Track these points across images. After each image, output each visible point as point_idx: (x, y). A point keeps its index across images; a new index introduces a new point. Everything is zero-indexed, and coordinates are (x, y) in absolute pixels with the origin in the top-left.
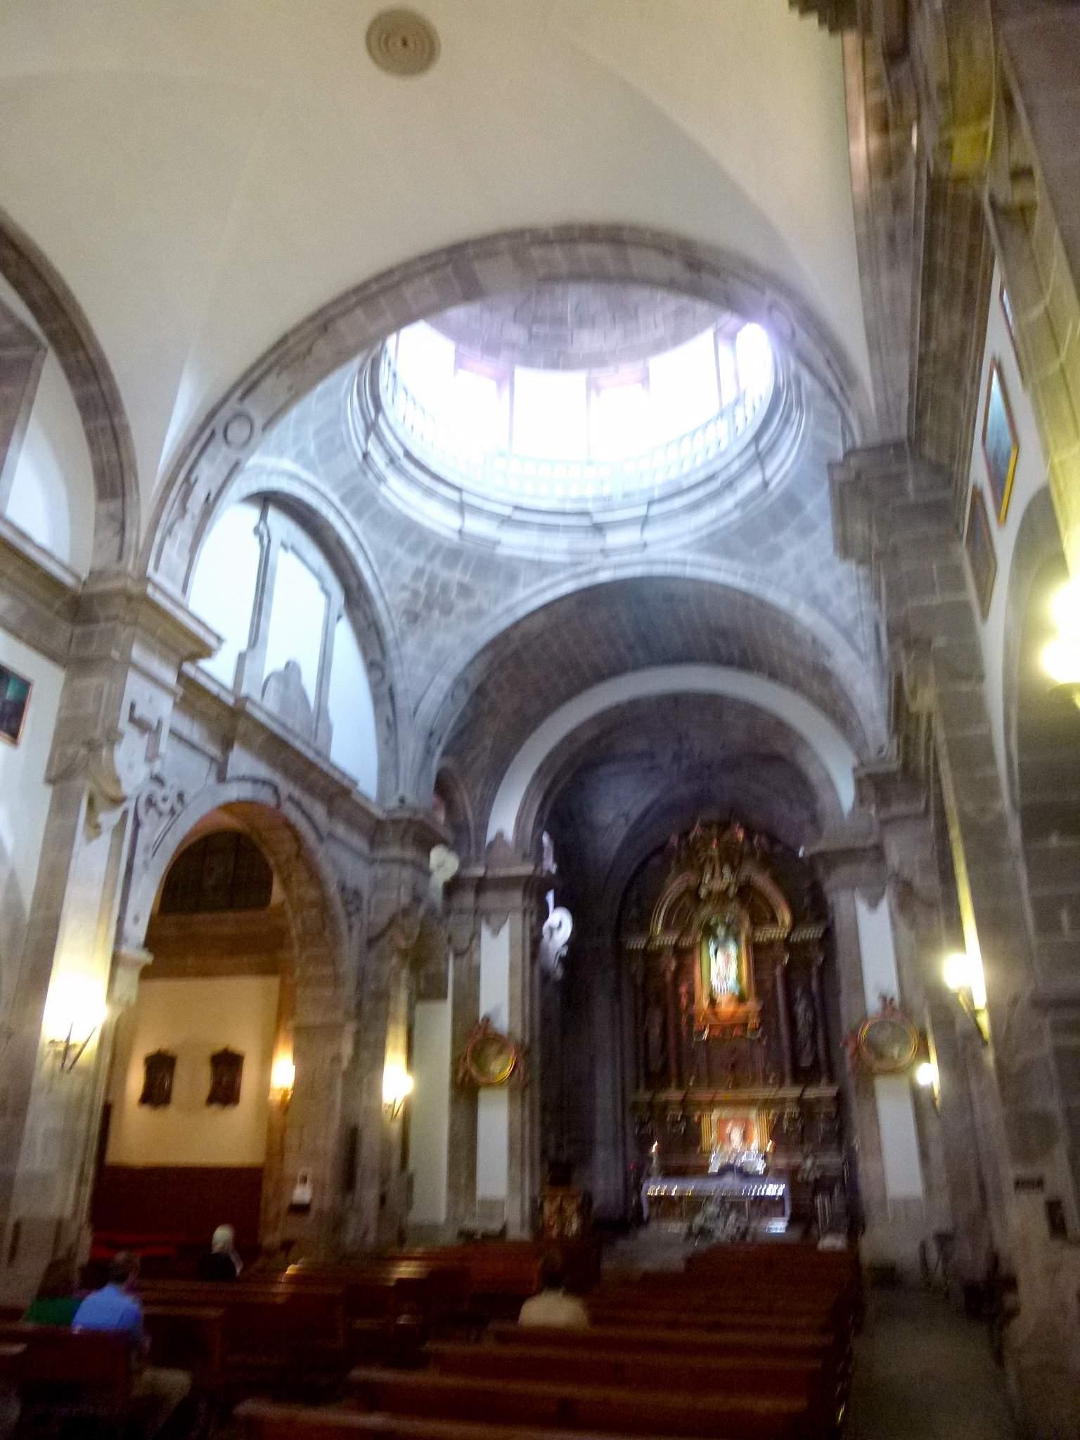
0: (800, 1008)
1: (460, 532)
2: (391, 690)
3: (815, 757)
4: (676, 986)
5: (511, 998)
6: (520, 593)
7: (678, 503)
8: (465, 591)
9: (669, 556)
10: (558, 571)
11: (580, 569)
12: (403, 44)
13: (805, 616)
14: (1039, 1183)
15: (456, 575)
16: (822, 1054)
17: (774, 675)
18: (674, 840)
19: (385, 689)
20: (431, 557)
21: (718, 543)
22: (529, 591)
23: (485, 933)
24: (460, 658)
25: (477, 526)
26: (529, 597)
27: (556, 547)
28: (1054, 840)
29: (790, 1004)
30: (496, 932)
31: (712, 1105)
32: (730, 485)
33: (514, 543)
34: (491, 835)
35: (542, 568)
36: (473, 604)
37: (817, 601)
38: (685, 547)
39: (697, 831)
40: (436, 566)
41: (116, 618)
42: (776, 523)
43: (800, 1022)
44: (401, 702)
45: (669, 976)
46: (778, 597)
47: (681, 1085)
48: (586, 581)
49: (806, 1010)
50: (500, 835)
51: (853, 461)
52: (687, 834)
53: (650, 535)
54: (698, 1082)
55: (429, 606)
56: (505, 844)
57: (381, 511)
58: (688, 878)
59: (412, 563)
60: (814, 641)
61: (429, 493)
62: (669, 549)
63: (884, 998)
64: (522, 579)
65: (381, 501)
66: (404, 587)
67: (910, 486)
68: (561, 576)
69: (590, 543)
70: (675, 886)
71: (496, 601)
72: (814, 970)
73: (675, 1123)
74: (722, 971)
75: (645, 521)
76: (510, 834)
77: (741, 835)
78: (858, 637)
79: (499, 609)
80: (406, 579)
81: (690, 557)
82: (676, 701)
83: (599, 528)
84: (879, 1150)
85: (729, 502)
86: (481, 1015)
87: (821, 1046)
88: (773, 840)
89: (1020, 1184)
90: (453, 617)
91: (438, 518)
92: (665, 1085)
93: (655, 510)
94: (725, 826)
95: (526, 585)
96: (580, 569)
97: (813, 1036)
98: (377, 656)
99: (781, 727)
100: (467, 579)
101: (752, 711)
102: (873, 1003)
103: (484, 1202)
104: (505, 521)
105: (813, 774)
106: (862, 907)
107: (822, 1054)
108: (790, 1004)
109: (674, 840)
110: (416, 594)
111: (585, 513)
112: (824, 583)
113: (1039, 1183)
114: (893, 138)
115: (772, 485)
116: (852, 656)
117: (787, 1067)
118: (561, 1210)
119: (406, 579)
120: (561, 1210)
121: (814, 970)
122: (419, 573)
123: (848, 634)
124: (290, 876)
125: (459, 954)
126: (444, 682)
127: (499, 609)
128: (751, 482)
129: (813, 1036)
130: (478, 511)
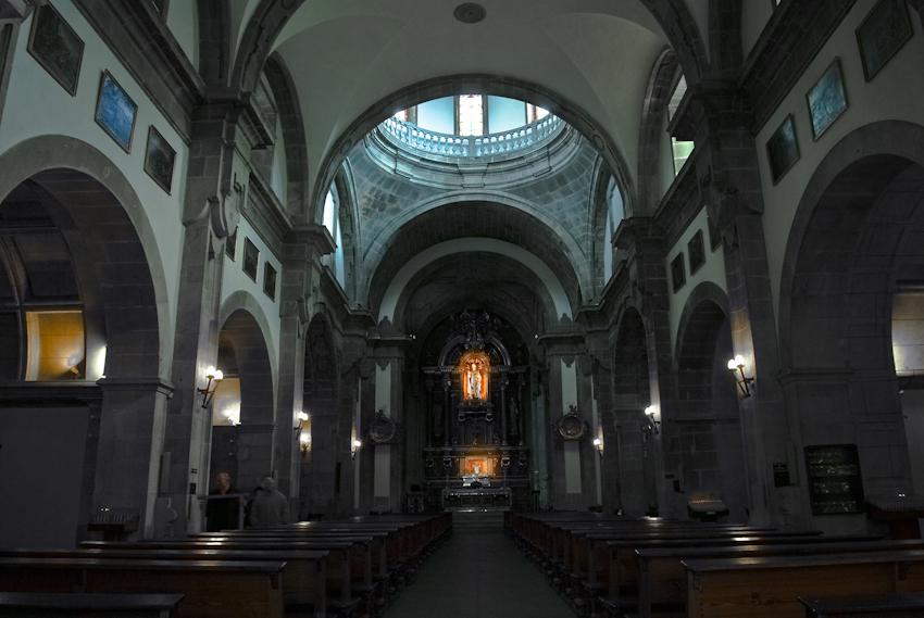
0: (513, 408)
1: (394, 170)
2: (354, 249)
3: (547, 291)
5: (392, 401)
6: (419, 203)
7: (502, 167)
8: (392, 199)
9: (496, 192)
10: (439, 193)
11: (450, 193)
12: (470, 14)
13: (559, 231)
14: (672, 476)
15: (389, 192)
16: (521, 430)
17: (539, 255)
18: (452, 318)
19: (350, 248)
20: (380, 183)
21: (520, 190)
22: (423, 202)
23: (378, 368)
24: (388, 233)
25: (402, 168)
26: (423, 205)
27: (438, 181)
28: (688, 370)
29: (508, 403)
30: (383, 369)
31: (467, 454)
32: (530, 164)
33: (417, 177)
34: (380, 319)
35: (431, 190)
36: (395, 206)
37: (565, 225)
38: (502, 189)
39: (465, 313)
40: (380, 187)
41: (305, 242)
42: (552, 187)
43: (512, 415)
44: (359, 255)
46: (543, 219)
47: (450, 445)
48: (453, 200)
50: (386, 317)
51: (632, 221)
52: (459, 314)
53: (486, 181)
54: (459, 443)
55: (374, 206)
56: (389, 322)
57: (363, 161)
58: (460, 338)
59: (371, 184)
60: (561, 242)
61: (383, 150)
62: (495, 189)
63: (571, 407)
64: (421, 196)
65: (365, 157)
66: (365, 197)
67: (650, 233)
68: (440, 196)
69: (457, 181)
70: (451, 342)
71: (406, 205)
72: (520, 388)
73: (448, 462)
74: (475, 382)
75: (484, 173)
76: (391, 318)
77: (488, 317)
78: (583, 246)
79: (408, 209)
80: (366, 193)
81: (506, 195)
82: (479, 255)
83: (461, 173)
84: (564, 474)
85: (529, 171)
86: (377, 411)
87: (521, 425)
88: (503, 320)
89: (667, 477)
90: (385, 213)
91: (386, 163)
92: (443, 444)
93: (490, 168)
94: (479, 312)
95: (422, 199)
96: (450, 193)
97: (518, 421)
98: (349, 232)
99: (531, 275)
100: (394, 194)
101: (517, 264)
102: (566, 410)
103: (378, 499)
104: (415, 166)
105: (545, 300)
106: (563, 365)
107: (521, 430)
108: (508, 403)
109: (452, 318)
110: (370, 199)
111: (455, 165)
112: (570, 217)
113: (672, 476)
114: (661, 100)
115: (554, 169)
116: (580, 254)
117: (504, 436)
118: (416, 501)
119: (366, 193)
120: (416, 501)
121: (520, 388)
122: (373, 189)
123: (578, 243)
124: (314, 344)
125: (364, 379)
126: (378, 245)
127: (408, 209)
128: (543, 166)
129: (518, 421)
130: (404, 160)
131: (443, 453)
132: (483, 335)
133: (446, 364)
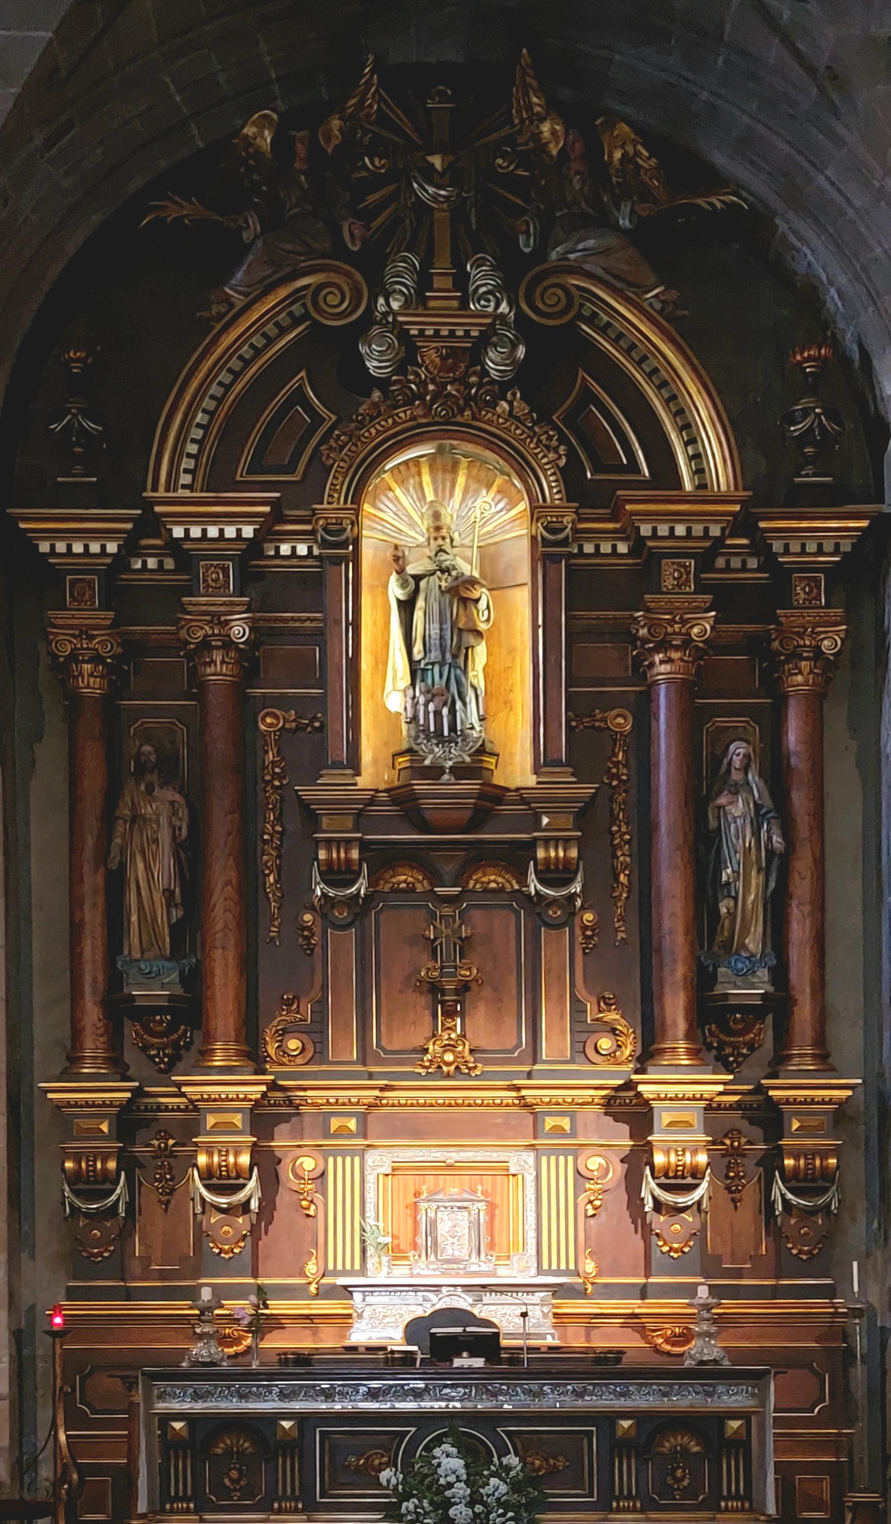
4: (244, 710)
29: (704, 782)
45: (218, 669)
49: (758, 818)
70: (253, 323)
121: (799, 680)
129: (777, 907)
131: (461, 1400)
132: (514, 275)
133: (217, 477)
